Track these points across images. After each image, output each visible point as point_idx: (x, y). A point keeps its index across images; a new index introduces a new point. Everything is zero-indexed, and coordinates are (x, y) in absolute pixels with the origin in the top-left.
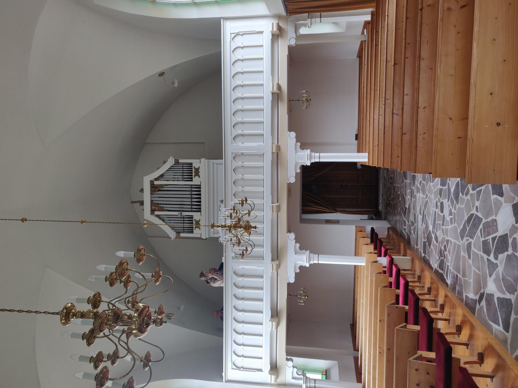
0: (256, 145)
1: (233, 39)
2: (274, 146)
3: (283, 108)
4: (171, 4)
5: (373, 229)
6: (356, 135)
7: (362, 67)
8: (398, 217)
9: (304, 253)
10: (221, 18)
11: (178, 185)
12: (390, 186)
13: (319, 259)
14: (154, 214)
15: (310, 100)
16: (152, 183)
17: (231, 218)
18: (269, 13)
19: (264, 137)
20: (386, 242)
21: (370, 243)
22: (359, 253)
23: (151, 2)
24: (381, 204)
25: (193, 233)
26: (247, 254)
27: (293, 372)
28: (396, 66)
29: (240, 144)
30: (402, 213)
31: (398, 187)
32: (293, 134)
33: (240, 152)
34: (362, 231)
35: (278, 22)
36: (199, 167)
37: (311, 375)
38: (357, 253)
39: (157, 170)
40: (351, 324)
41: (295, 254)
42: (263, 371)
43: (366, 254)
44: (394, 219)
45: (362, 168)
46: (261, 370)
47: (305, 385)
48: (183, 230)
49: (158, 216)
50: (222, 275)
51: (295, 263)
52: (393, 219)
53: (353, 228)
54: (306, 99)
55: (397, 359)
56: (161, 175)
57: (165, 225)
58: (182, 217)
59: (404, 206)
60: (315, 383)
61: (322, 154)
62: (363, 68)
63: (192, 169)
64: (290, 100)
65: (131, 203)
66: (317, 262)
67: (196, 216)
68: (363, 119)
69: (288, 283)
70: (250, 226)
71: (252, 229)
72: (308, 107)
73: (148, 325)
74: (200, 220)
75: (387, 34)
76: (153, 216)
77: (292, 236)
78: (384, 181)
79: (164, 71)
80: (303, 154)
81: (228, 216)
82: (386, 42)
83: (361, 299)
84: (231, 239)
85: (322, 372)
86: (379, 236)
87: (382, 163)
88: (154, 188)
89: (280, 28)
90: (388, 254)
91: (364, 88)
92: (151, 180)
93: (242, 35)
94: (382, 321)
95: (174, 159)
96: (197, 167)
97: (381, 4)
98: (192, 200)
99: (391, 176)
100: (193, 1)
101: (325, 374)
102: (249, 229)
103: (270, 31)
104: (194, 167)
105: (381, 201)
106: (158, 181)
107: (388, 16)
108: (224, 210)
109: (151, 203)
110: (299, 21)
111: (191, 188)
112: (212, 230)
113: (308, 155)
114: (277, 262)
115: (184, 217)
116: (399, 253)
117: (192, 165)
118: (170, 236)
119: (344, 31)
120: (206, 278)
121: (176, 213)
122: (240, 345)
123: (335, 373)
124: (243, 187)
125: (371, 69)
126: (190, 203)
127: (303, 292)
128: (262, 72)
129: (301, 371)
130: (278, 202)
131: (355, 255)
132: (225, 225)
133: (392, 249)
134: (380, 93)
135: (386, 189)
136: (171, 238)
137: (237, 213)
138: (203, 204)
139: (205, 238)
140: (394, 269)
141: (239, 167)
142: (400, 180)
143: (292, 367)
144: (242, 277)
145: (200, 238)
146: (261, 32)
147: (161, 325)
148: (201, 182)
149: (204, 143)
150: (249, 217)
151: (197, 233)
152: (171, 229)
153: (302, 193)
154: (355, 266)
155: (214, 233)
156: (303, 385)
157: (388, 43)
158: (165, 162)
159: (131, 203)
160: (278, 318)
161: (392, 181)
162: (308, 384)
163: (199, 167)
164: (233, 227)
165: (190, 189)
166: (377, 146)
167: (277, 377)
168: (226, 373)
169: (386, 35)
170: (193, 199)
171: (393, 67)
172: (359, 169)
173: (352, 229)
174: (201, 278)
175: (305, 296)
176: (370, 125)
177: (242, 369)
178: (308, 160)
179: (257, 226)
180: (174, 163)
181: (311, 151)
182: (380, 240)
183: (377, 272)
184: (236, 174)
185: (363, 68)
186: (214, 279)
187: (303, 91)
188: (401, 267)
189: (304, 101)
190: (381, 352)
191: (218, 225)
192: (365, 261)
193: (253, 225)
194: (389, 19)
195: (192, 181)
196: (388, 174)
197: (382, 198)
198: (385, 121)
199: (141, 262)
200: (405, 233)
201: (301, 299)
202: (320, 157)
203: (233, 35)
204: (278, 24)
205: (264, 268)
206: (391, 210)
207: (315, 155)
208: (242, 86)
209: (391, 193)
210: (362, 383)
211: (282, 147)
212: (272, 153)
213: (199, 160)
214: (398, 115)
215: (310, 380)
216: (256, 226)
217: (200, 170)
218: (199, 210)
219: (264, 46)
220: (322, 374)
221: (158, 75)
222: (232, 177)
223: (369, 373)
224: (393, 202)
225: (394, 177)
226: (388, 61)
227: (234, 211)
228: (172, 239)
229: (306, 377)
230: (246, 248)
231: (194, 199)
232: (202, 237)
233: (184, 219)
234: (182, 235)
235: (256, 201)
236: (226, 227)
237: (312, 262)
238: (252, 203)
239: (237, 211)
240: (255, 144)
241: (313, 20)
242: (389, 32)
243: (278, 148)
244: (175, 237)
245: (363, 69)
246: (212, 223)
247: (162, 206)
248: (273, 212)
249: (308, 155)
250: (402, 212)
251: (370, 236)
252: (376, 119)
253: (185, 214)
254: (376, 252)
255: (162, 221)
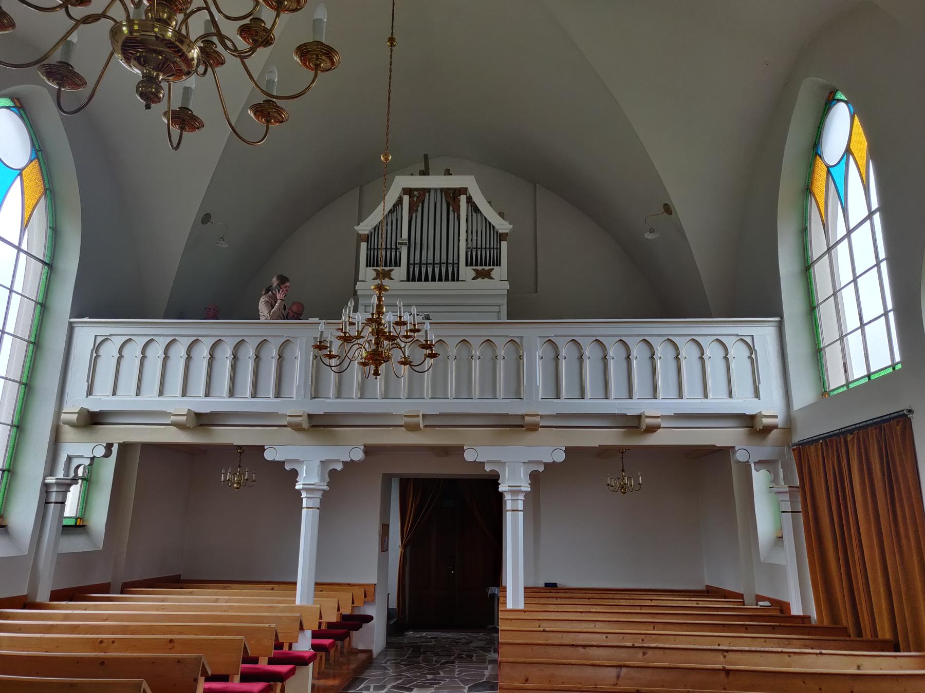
0: (538, 385)
1: (742, 340)
2: (538, 419)
3: (610, 437)
4: (804, 223)
5: (369, 619)
6: (556, 584)
7: (689, 596)
8: (393, 673)
9: (322, 480)
10: (782, 317)
11: (459, 240)
12: (455, 654)
13: (311, 510)
14: (404, 194)
15: (624, 493)
16: (464, 191)
17: (397, 323)
18: (795, 409)
19: (555, 401)
20: (342, 647)
21: (341, 614)
22: (321, 591)
23: (807, 185)
24: (418, 636)
25: (367, 266)
26: (322, 357)
27: (82, 457)
28: (723, 675)
29: (539, 353)
30: (400, 681)
31: (453, 671)
32: (560, 457)
33: (525, 353)
34: (365, 597)
35: (779, 427)
36: (493, 279)
37: (74, 494)
38: (321, 588)
39: (488, 202)
40: (180, 576)
41: (321, 461)
42: (87, 397)
43: (319, 606)
44: (388, 663)
45: (488, 596)
46: (90, 392)
47: (54, 481)
48: (372, 247)
49: (400, 201)
50: (282, 317)
51: (303, 462)
52: (388, 660)
53: (373, 580)
54: (625, 484)
55: (72, 685)
56: (478, 208)
57: (384, 214)
58: (398, 246)
59: (416, 686)
60: (56, 503)
61: (521, 514)
62: (690, 599)
63: (490, 265)
64: (622, 451)
65: (425, 155)
66: (304, 505)
67: (400, 272)
68: (589, 599)
69: (264, 446)
70: (381, 364)
71: (373, 367)
72: (612, 489)
73: (142, 62)
74: (392, 279)
75: (782, 652)
76: (399, 193)
77: (358, 455)
78: (463, 641)
79: (674, 214)
80: (522, 477)
81: (400, 317)
82: (766, 649)
83: (227, 597)
84: (354, 324)
85: (80, 519)
86: (354, 632)
87: (511, 641)
88: (452, 196)
89: (767, 430)
90: (316, 654)
91: (652, 600)
92: (469, 189)
93: (750, 357)
94: (171, 645)
95: (507, 231)
96: (493, 274)
97: (836, 638)
98: (430, 265)
99: (475, 655)
100: (812, 263)
101: (78, 524)
102: (372, 360)
103: (761, 412)
104: (493, 269)
105: (424, 634)
106: (467, 202)
107: (821, 654)
108: (414, 311)
109: (424, 189)
110: (782, 468)
111: (454, 264)
112: (373, 287)
113: (521, 486)
114: (305, 425)
115: (398, 250)
116: (318, 675)
117: (497, 265)
118: (361, 224)
119: (762, 559)
120: (276, 287)
121: (405, 235)
122: (143, 352)
123: (76, 544)
124: (456, 358)
125: (694, 616)
126: (424, 261)
127: (247, 480)
128: (681, 396)
129: (86, 475)
130: (426, 426)
131: (317, 584)
132: (383, 313)
133: (327, 660)
134: (653, 636)
135: (447, 646)
136: (358, 224)
137: (407, 337)
138: (423, 285)
139: (356, 289)
140: (283, 668)
141: (494, 351)
142: (466, 675)
143: (92, 456)
144: (279, 356)
145: (356, 280)
146: (757, 395)
147: (142, 95)
148: (465, 281)
149: (536, 292)
150: (398, 362)
151: (367, 274)
152: (376, 226)
153: (440, 479)
154: (295, 584)
155: (365, 306)
156: (55, 478)
157: (763, 655)
158: (501, 215)
159: (425, 155)
160: (193, 427)
161: (463, 657)
162: (55, 489)
163: (493, 279)
164: (377, 329)
165: (450, 261)
166: (542, 629)
167: (73, 425)
168: (88, 325)
169: (780, 650)
170: (431, 266)
171: (720, 667)
172: (487, 590)
173: (371, 578)
174: (277, 278)
175: (239, 483)
176: (581, 612)
177: (95, 355)
178: (509, 486)
179: (378, 377)
180: (500, 231)
181: (527, 494)
182: (348, 635)
183: (278, 631)
184: (482, 344)
185: (690, 599)
186: (273, 302)
187: (640, 477)
188: (290, 683)
189: (621, 481)
190: (103, 645)
191: (383, 299)
192: (305, 604)
193: (382, 368)
194: (815, 656)
195: (467, 265)
196: (477, 649)
197: (430, 637)
198: (598, 646)
199: (301, 59)
200: (360, 687)
201: (234, 474)
202: (516, 512)
203: (749, 340)
204: (775, 427)
205: (295, 399)
206: (406, 656)
207: (519, 501)
208: (652, 358)
209: (441, 655)
210: (50, 601)
211: (532, 437)
212: (523, 416)
213: (506, 279)
214: (618, 677)
215: (63, 492)
216: (379, 375)
217: (486, 279)
218: (410, 278)
219: (730, 400)
220: (77, 519)
221: (666, 203)
222: (477, 337)
223: (67, 617)
224: (422, 660)
225: (472, 662)
226: (725, 654)
227: (411, 331)
228: (356, 228)
229: (70, 485)
230: (334, 356)
231: (431, 269)
232: (358, 283)
233: (394, 250)
234: (364, 246)
235: (427, 377)
236: (379, 315)
237: (304, 495)
238: (425, 368)
239: (410, 337)
240: (539, 381)
241: (787, 497)
242: (786, 657)
243: (533, 428)
244: (360, 232)
245: (688, 599)
246: (386, 287)
247: (420, 209)
248: (405, 416)
249: (521, 486)
250: (402, 680)
251: (355, 614)
252: (595, 626)
253: (404, 251)
254: (323, 627)
255: (391, 209)
